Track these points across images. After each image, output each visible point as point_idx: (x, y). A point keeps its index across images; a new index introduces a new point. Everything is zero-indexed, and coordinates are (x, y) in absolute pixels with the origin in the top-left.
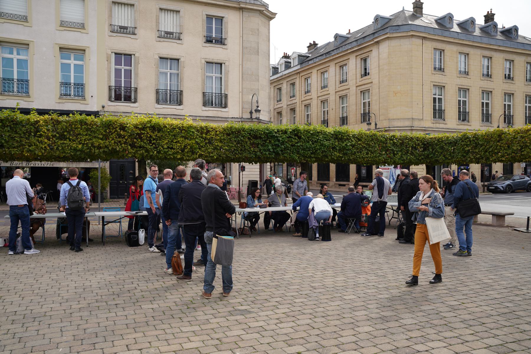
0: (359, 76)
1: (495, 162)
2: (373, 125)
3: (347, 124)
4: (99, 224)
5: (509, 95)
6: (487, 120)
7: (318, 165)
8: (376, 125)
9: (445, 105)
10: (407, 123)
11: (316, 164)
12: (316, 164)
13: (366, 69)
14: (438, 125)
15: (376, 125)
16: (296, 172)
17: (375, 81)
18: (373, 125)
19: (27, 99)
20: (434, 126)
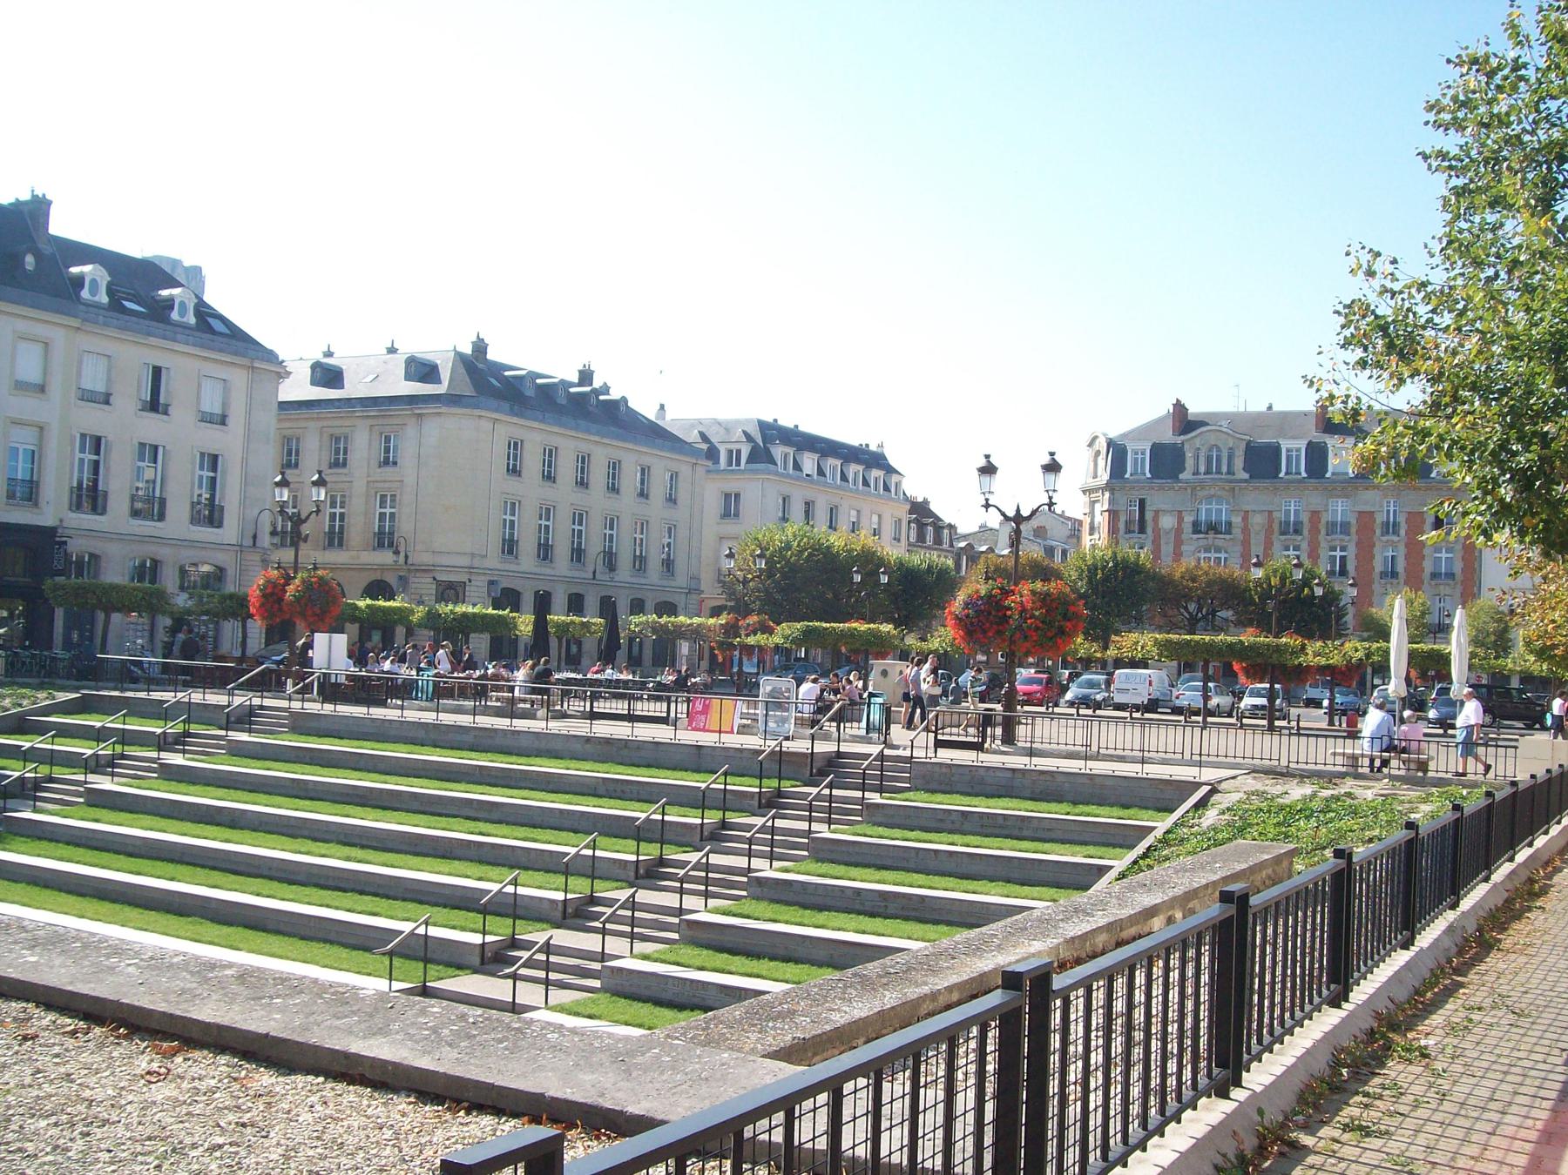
0: (374, 463)
1: (226, 618)
2: (402, 555)
3: (341, 545)
4: (1157, 512)
5: (547, 513)
6: (510, 552)
7: (66, 612)
8: (406, 557)
9: (167, 384)
10: (465, 561)
11: (61, 609)
12: (61, 609)
13: (387, 450)
14: (508, 567)
15: (406, 557)
16: (1178, 555)
17: (410, 480)
18: (402, 555)
19: (35, 510)
20: (537, 570)
